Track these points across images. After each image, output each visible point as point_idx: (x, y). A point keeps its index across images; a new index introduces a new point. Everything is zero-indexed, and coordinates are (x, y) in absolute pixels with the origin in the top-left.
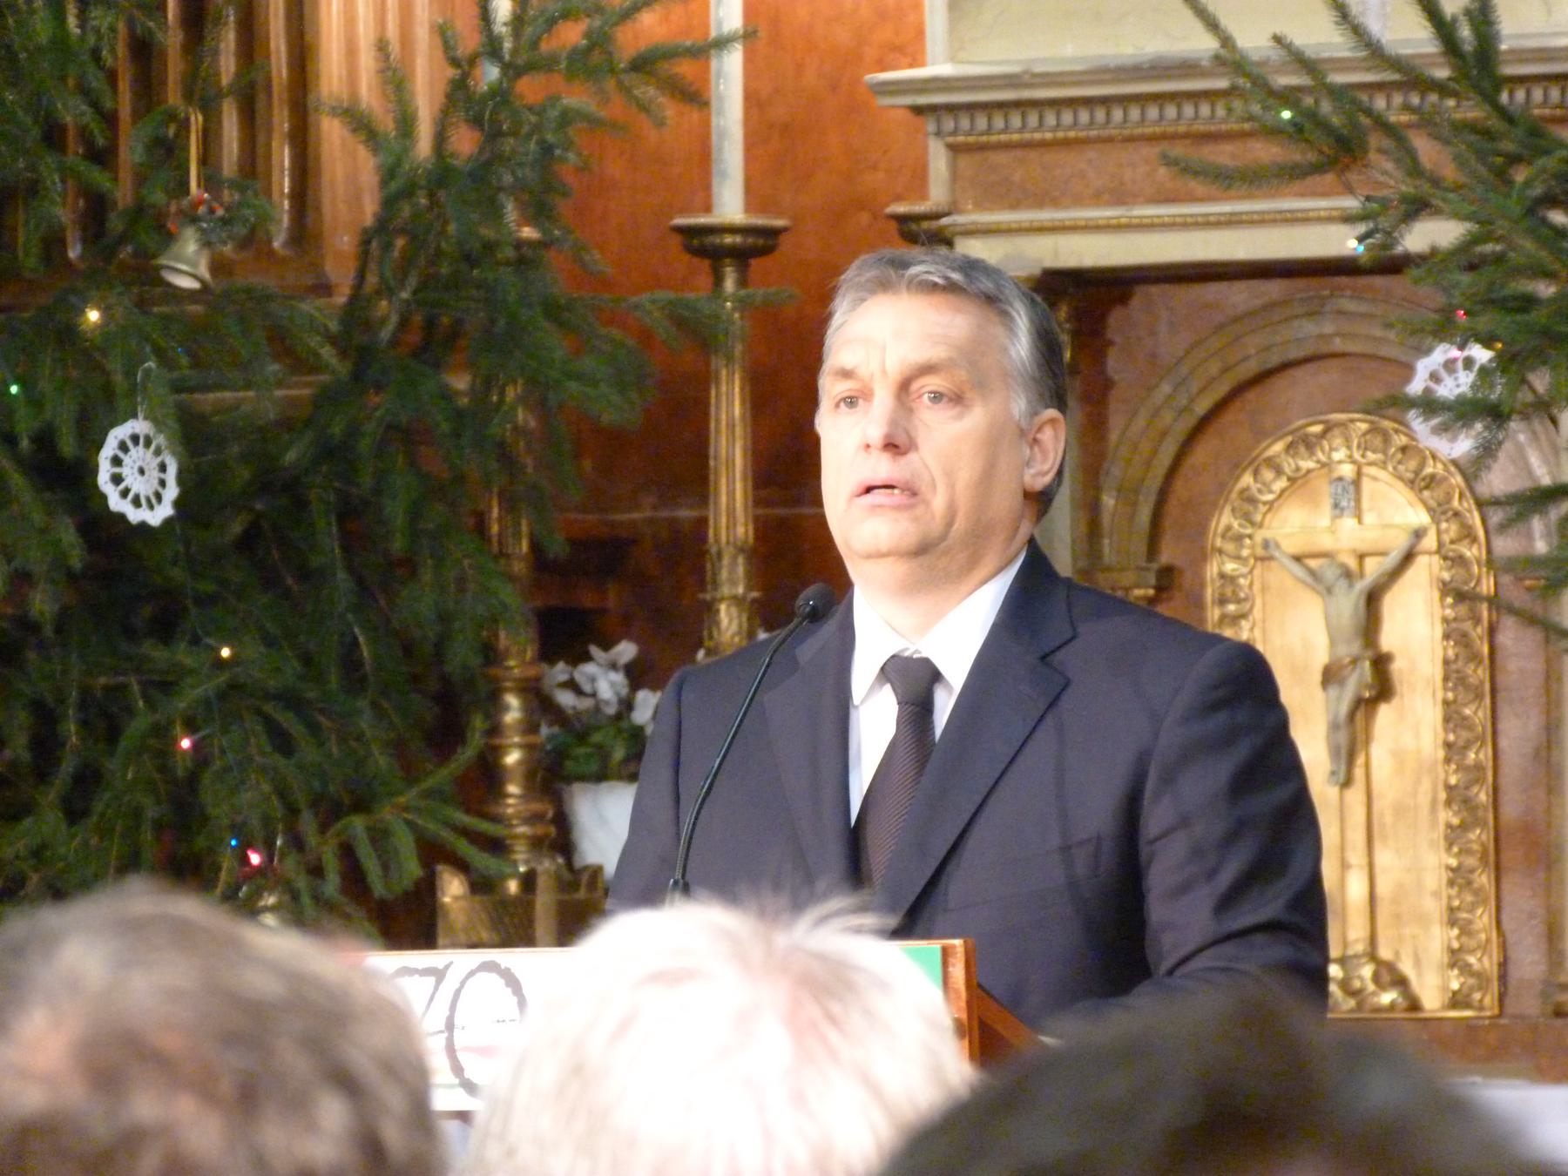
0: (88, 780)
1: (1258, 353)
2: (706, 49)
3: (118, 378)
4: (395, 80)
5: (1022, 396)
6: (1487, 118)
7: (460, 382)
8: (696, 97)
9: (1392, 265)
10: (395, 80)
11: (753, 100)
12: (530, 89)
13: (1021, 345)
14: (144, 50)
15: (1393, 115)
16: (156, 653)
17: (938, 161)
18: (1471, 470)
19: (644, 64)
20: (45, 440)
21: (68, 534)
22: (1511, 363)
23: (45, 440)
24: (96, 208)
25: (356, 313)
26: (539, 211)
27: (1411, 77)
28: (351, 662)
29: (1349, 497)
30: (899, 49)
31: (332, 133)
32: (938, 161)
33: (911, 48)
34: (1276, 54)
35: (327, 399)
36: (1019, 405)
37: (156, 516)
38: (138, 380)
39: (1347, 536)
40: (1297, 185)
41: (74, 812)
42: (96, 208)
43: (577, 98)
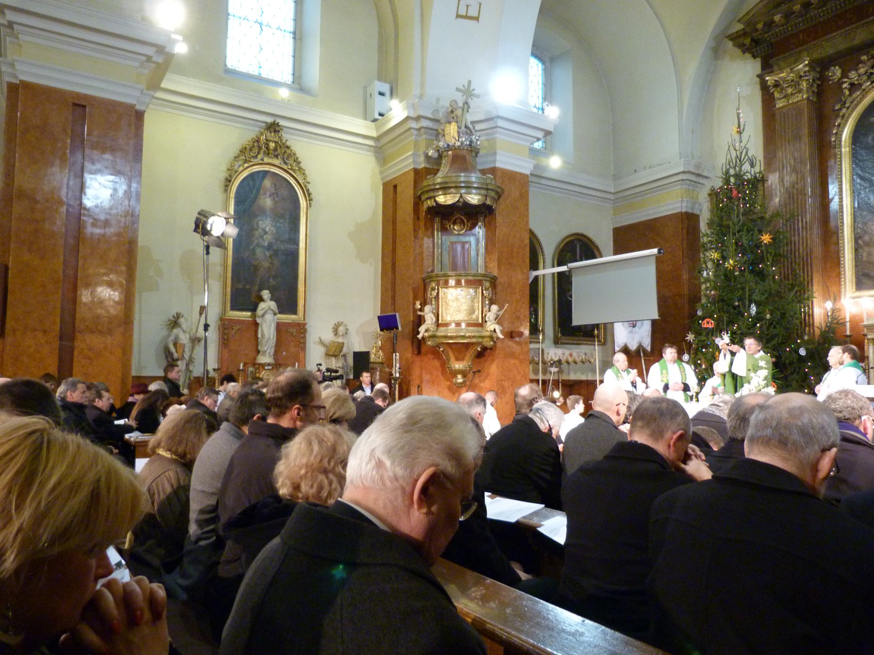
0: (798, 373)
2: (846, 322)
3: (309, 473)
6: (702, 233)
7: (826, 345)
8: (845, 326)
11: (850, 326)
12: (832, 325)
15: (782, 180)
16: (803, 364)
17: (865, 330)
19: (841, 323)
20: (795, 349)
21: (797, 356)
23: (795, 349)
26: (833, 333)
28: (819, 365)
30: (537, 351)
32: (865, 330)
33: (863, 322)
35: (816, 347)
37: (804, 355)
38: (158, 519)
40: (859, 440)
41: (797, 375)
43: (836, 326)
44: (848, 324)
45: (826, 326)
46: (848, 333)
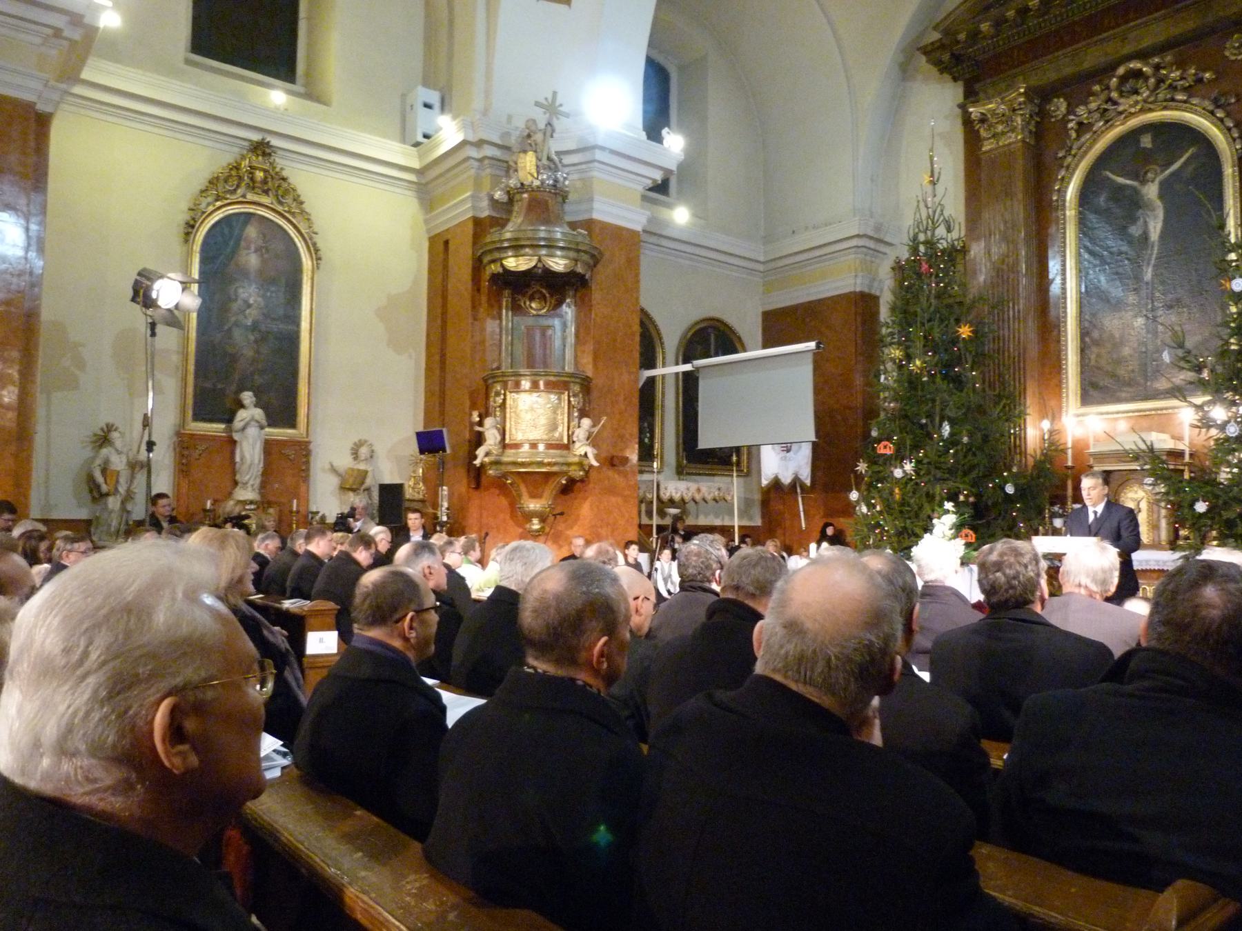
1: (447, 566)
4: (1035, 452)
5: (92, 800)
8: (1066, 454)
9: (1143, 470)
10: (1035, 452)
13: (1100, 481)
14: (1010, 449)
18: (1151, 491)
22: (1156, 480)
24: (1005, 464)
25: (1032, 474)
27: (1144, 451)
29: (1136, 492)
31: (1028, 457)
34: (1183, 383)
36: (1101, 487)
39: (1135, 496)
42: (1005, 464)
43: (1054, 454)
44: (1070, 452)
45: (1042, 454)
46: (1070, 464)
